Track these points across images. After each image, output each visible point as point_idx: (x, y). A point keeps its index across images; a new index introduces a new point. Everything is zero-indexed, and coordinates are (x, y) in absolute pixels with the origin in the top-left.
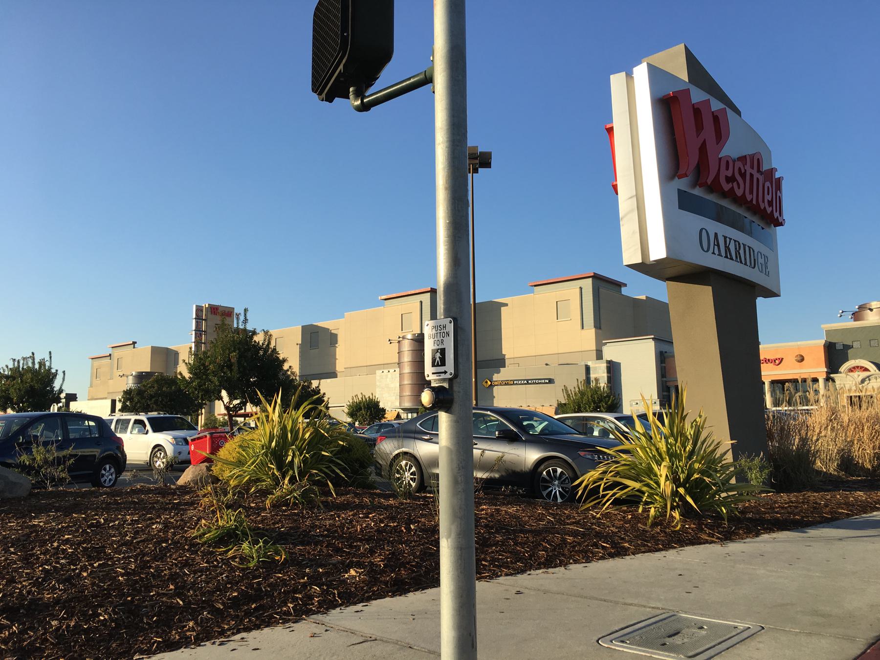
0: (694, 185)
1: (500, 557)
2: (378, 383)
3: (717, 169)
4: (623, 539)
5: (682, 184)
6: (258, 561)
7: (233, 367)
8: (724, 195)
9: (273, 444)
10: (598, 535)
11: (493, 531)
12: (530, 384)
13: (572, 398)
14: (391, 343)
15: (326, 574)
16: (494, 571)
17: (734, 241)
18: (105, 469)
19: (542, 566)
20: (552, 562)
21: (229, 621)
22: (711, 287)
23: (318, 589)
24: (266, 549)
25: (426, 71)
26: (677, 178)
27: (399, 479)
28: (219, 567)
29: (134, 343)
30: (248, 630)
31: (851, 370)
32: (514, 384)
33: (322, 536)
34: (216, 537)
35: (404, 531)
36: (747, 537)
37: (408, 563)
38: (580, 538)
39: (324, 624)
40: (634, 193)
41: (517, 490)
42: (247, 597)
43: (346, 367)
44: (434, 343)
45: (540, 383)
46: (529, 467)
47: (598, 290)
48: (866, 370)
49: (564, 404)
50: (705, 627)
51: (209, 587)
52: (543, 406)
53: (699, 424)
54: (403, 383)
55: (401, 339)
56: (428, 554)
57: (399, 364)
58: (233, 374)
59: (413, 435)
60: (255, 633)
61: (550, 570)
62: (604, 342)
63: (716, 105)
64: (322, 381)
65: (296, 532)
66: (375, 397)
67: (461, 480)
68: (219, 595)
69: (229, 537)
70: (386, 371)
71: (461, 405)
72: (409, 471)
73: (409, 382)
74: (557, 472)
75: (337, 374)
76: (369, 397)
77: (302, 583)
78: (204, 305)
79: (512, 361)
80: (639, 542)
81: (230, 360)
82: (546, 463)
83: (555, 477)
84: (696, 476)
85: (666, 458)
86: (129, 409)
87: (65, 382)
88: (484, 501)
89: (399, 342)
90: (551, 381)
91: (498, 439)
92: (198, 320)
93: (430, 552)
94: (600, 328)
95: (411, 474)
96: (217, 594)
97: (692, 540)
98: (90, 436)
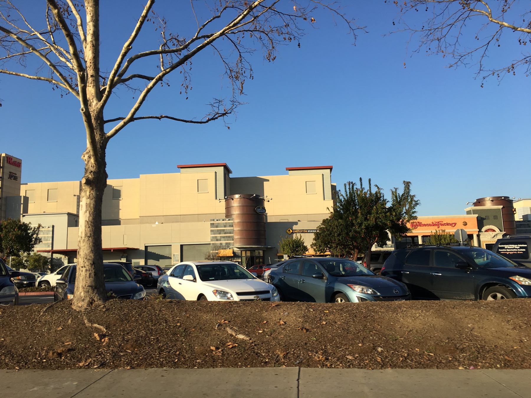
31: (486, 231)
32: (308, 232)
48: (494, 231)
75: (120, 221)
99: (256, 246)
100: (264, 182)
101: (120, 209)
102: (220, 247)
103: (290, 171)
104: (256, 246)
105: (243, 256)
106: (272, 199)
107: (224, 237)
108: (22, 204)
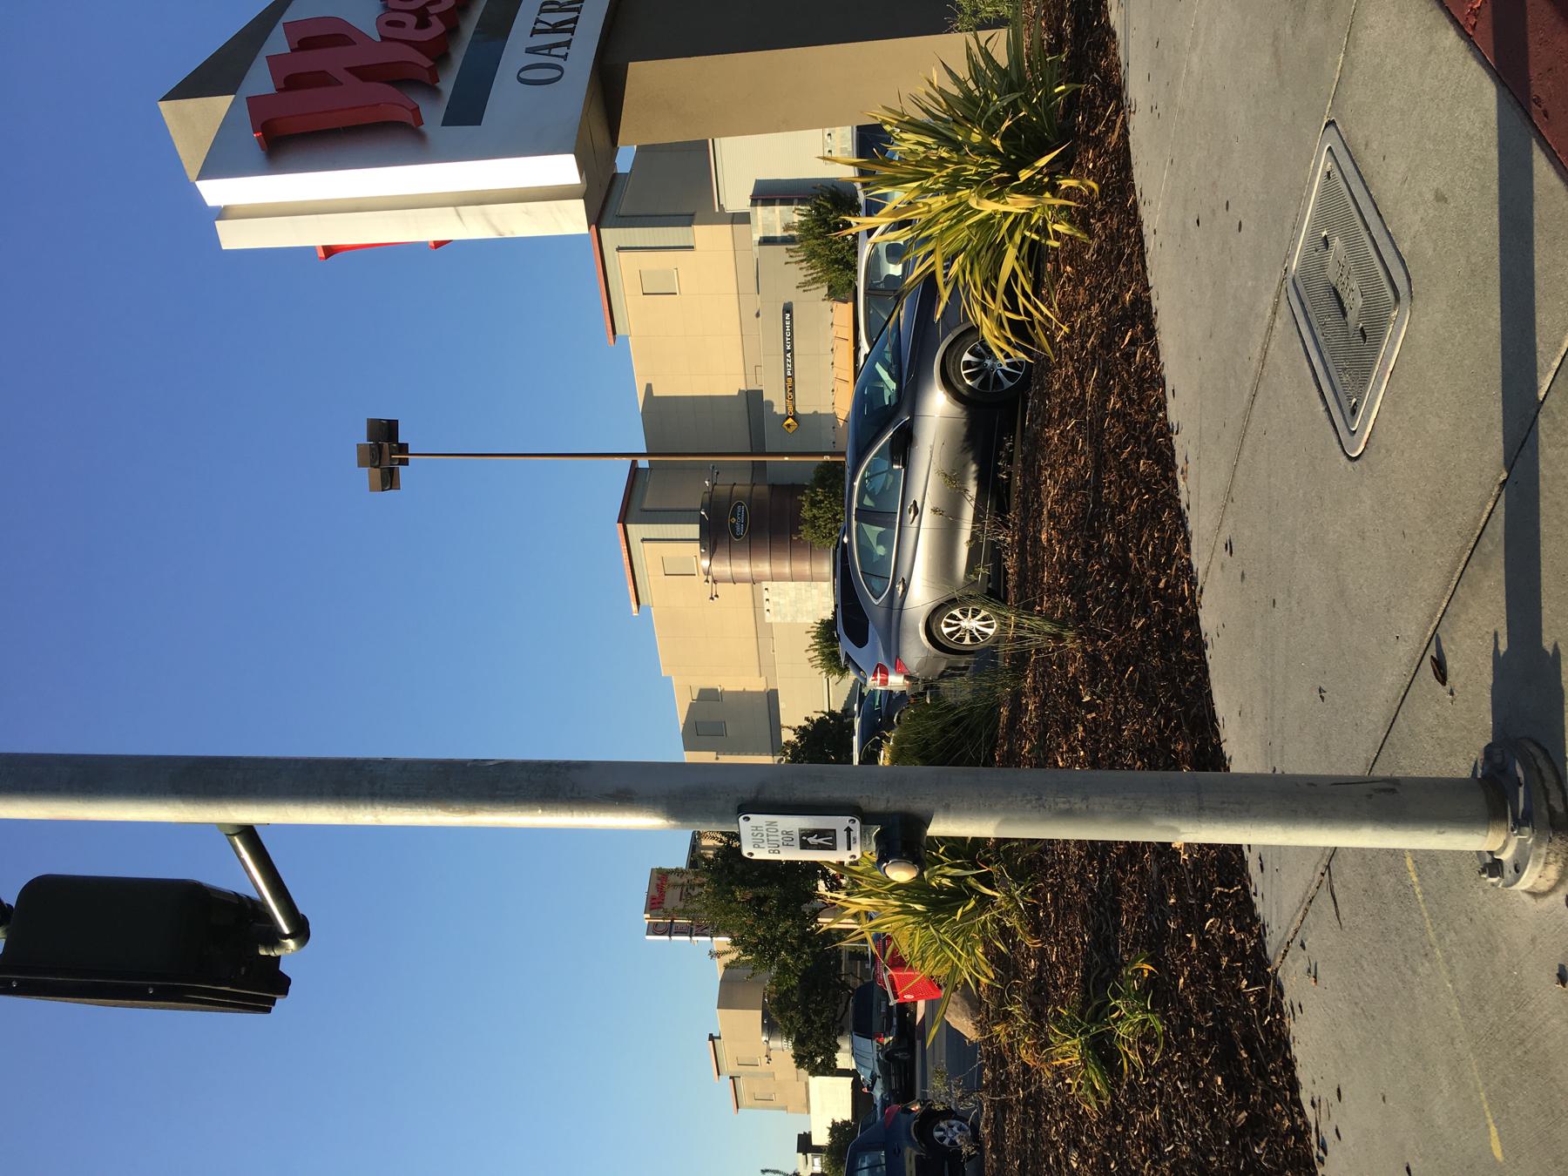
0: (433, 90)
1: (1150, 549)
2: (789, 619)
3: (405, 46)
4: (1115, 299)
5: (432, 114)
6: (1153, 1012)
7: (762, 895)
8: (453, 30)
9: (919, 907)
10: (1107, 343)
11: (1096, 545)
12: (792, 346)
13: (820, 274)
14: (717, 596)
15: (1180, 892)
16: (1177, 569)
17: (542, 15)
18: (942, 1139)
19: (1170, 475)
20: (1162, 453)
21: (1275, 1112)
22: (630, 63)
23: (1211, 920)
24: (1130, 994)
25: (227, 835)
26: (422, 127)
27: (973, 639)
28: (1163, 1087)
29: (712, 1038)
30: (1294, 1086)
32: (792, 377)
33: (1101, 872)
34: (1101, 1070)
35: (1094, 715)
36: (1115, 55)
37: (1161, 732)
38: (1112, 382)
39: (1288, 943)
40: (452, 208)
41: (1007, 451)
42: (1226, 1061)
43: (758, 674)
44: (787, 845)
45: (791, 328)
46: (959, 410)
47: (623, 216)
49: (829, 290)
50: (1324, 233)
51: (1204, 1123)
52: (832, 324)
53: (896, 122)
54: (789, 575)
55: (710, 578)
56: (1143, 687)
57: (754, 581)
58: (773, 895)
59: (895, 612)
60: (1302, 1074)
61: (1179, 461)
62: (717, 210)
63: (278, 43)
64: (783, 722)
65: (1093, 917)
66: (812, 627)
67: (1064, 803)
68: (1220, 1110)
69: (1103, 1052)
70: (767, 605)
71: (914, 798)
72: (960, 620)
73: (787, 564)
74: (969, 362)
75: (771, 690)
76: (813, 637)
77: (1198, 946)
78: (647, 921)
79: (751, 378)
80: (1123, 270)
81: (749, 902)
82: (954, 380)
83: (978, 364)
84: (997, 142)
85: (960, 197)
86: (829, 1058)
87: (780, 1169)
88: (1031, 530)
89: (715, 582)
90: (788, 309)
91: (906, 464)
92: (673, 930)
93: (1139, 682)
94: (693, 215)
95: (965, 615)
96: (1217, 1113)
97: (1119, 163)
98: (884, 1167)
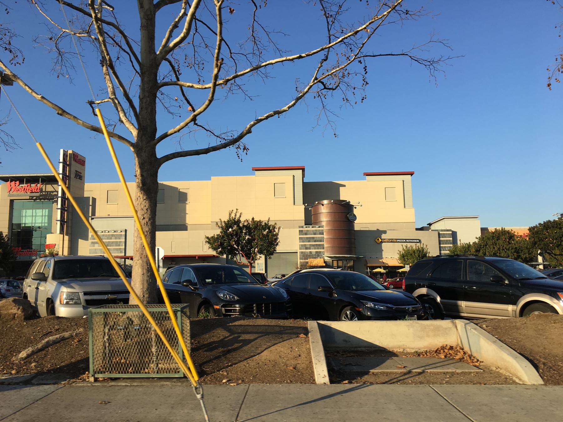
32: (397, 242)
43: (213, 221)
75: (187, 226)
99: (349, 256)
100: (340, 188)
101: (187, 214)
102: (309, 256)
103: (256, 172)
104: (349, 256)
105: (334, 266)
106: (361, 206)
107: (313, 245)
108: (90, 205)
